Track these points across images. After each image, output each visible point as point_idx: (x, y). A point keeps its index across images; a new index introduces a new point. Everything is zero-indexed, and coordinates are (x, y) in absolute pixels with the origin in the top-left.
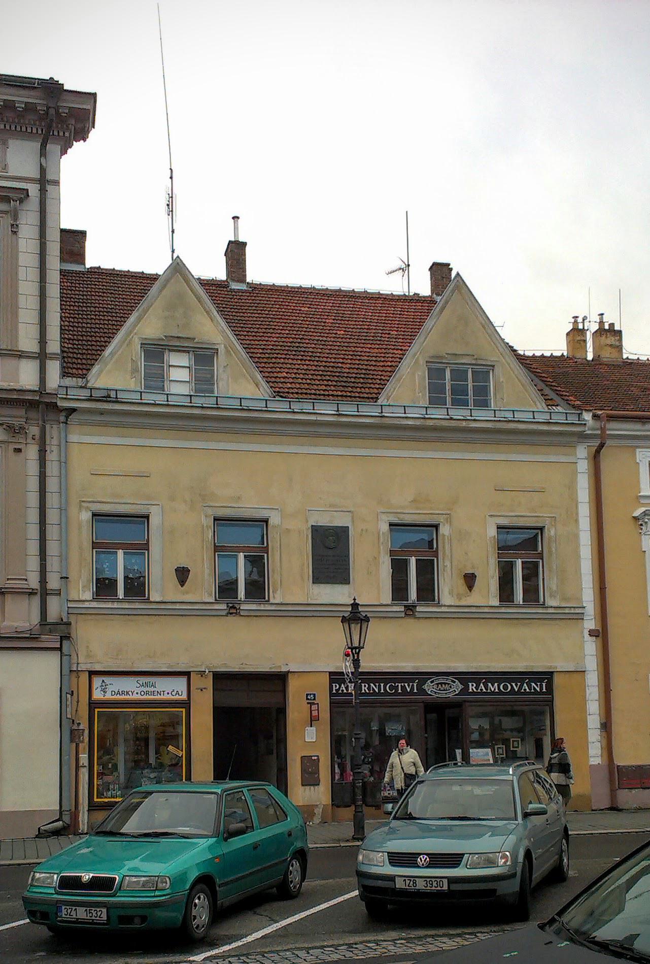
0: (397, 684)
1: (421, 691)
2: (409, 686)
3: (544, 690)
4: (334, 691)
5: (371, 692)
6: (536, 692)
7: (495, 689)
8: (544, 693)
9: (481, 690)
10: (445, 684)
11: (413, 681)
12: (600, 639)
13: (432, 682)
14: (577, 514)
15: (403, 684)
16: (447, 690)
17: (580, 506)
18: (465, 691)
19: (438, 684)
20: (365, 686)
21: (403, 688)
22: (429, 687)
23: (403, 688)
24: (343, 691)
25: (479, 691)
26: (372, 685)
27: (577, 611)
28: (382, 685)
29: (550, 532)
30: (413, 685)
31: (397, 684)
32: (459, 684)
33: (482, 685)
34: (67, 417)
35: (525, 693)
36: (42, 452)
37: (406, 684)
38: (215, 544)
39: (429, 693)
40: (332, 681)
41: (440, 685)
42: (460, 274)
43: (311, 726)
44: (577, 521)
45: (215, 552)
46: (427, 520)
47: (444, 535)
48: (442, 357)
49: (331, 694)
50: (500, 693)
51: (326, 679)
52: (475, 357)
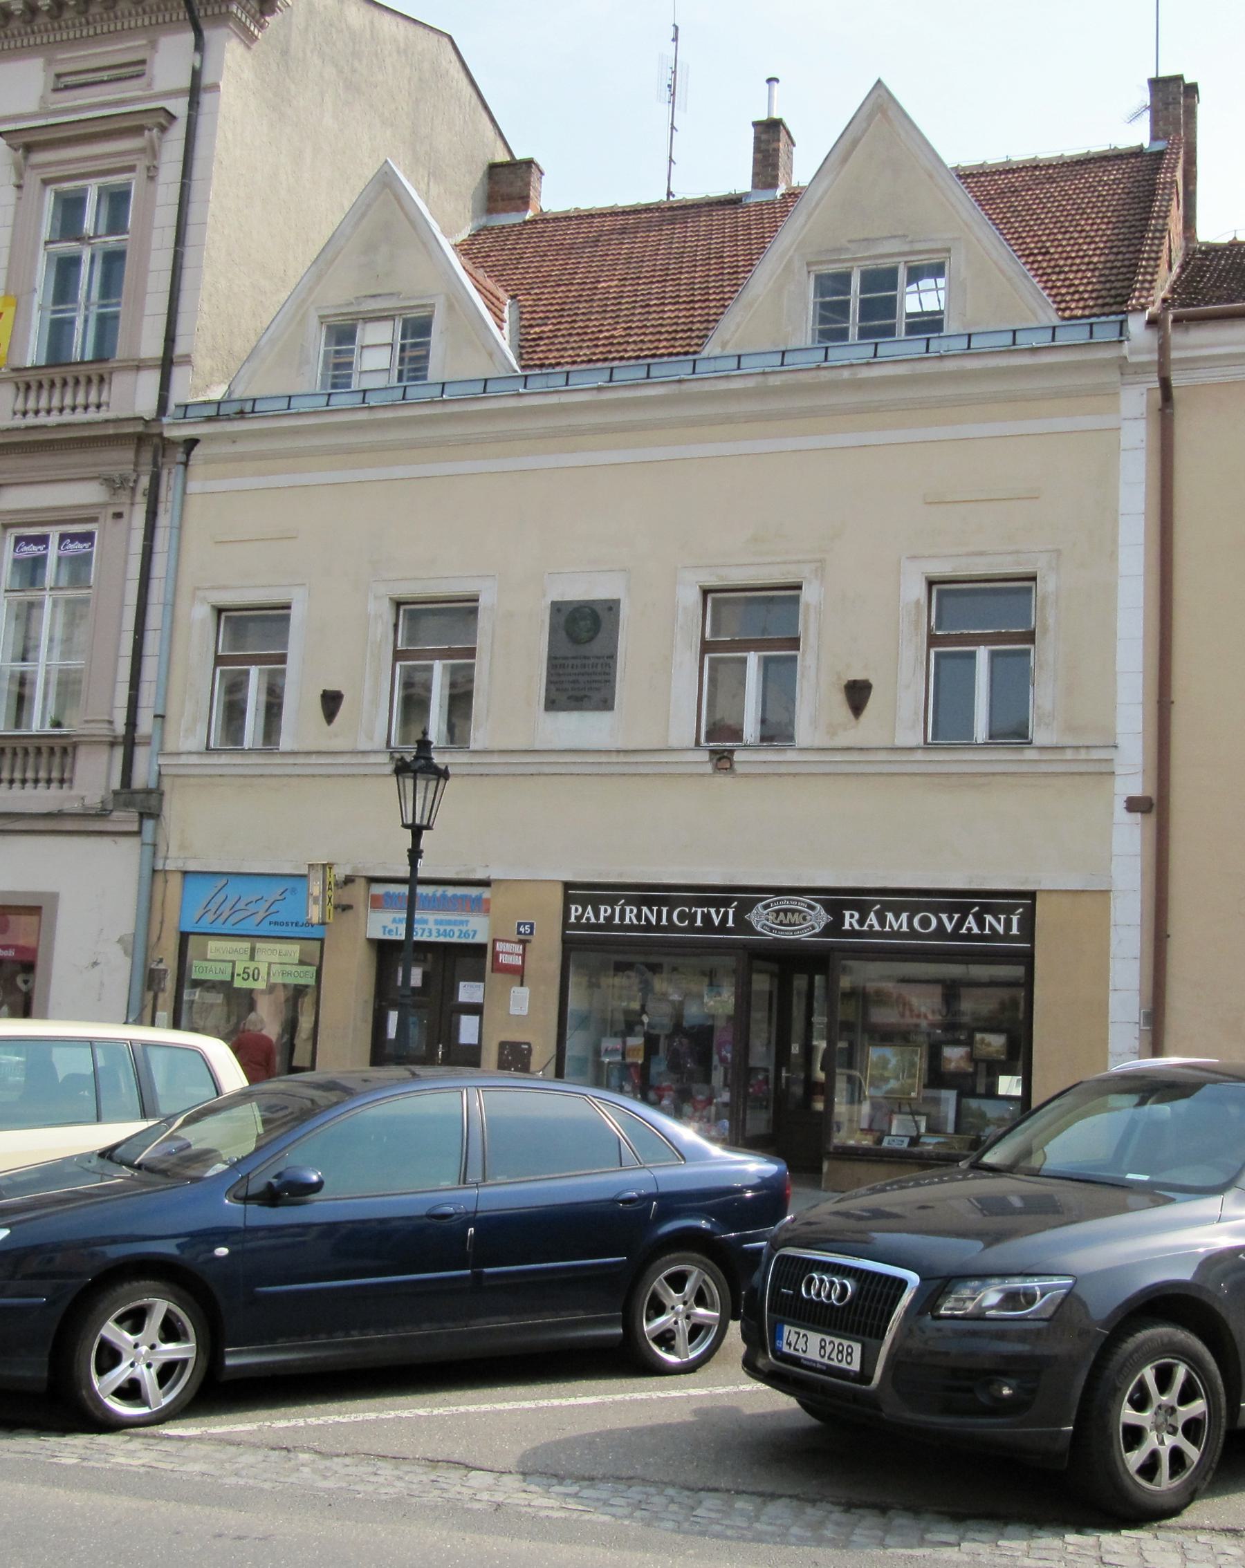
0: (694, 909)
1: (743, 926)
2: (718, 913)
3: (1015, 931)
4: (573, 920)
5: (643, 922)
6: (995, 935)
7: (901, 926)
8: (1014, 939)
9: (871, 926)
10: (793, 911)
11: (726, 903)
12: (1152, 819)
13: (766, 907)
14: (1115, 541)
15: (705, 910)
16: (795, 925)
17: (1122, 521)
18: (834, 928)
19: (777, 912)
20: (631, 911)
21: (707, 918)
22: (759, 918)
23: (707, 918)
24: (588, 919)
25: (865, 928)
26: (645, 909)
27: (1096, 755)
28: (665, 910)
29: (1046, 586)
30: (726, 913)
31: (694, 909)
32: (823, 912)
33: (872, 915)
34: (188, 454)
35: (970, 936)
36: (152, 515)
37: (713, 911)
38: (395, 645)
39: (759, 929)
40: (568, 901)
41: (782, 914)
42: (887, 82)
43: (522, 985)
44: (1113, 556)
45: (930, 645)
46: (791, 579)
47: (807, 605)
48: (839, 250)
49: (566, 924)
50: (913, 934)
51: (558, 895)
52: (909, 239)
